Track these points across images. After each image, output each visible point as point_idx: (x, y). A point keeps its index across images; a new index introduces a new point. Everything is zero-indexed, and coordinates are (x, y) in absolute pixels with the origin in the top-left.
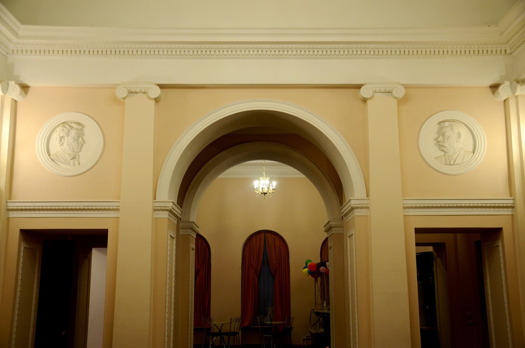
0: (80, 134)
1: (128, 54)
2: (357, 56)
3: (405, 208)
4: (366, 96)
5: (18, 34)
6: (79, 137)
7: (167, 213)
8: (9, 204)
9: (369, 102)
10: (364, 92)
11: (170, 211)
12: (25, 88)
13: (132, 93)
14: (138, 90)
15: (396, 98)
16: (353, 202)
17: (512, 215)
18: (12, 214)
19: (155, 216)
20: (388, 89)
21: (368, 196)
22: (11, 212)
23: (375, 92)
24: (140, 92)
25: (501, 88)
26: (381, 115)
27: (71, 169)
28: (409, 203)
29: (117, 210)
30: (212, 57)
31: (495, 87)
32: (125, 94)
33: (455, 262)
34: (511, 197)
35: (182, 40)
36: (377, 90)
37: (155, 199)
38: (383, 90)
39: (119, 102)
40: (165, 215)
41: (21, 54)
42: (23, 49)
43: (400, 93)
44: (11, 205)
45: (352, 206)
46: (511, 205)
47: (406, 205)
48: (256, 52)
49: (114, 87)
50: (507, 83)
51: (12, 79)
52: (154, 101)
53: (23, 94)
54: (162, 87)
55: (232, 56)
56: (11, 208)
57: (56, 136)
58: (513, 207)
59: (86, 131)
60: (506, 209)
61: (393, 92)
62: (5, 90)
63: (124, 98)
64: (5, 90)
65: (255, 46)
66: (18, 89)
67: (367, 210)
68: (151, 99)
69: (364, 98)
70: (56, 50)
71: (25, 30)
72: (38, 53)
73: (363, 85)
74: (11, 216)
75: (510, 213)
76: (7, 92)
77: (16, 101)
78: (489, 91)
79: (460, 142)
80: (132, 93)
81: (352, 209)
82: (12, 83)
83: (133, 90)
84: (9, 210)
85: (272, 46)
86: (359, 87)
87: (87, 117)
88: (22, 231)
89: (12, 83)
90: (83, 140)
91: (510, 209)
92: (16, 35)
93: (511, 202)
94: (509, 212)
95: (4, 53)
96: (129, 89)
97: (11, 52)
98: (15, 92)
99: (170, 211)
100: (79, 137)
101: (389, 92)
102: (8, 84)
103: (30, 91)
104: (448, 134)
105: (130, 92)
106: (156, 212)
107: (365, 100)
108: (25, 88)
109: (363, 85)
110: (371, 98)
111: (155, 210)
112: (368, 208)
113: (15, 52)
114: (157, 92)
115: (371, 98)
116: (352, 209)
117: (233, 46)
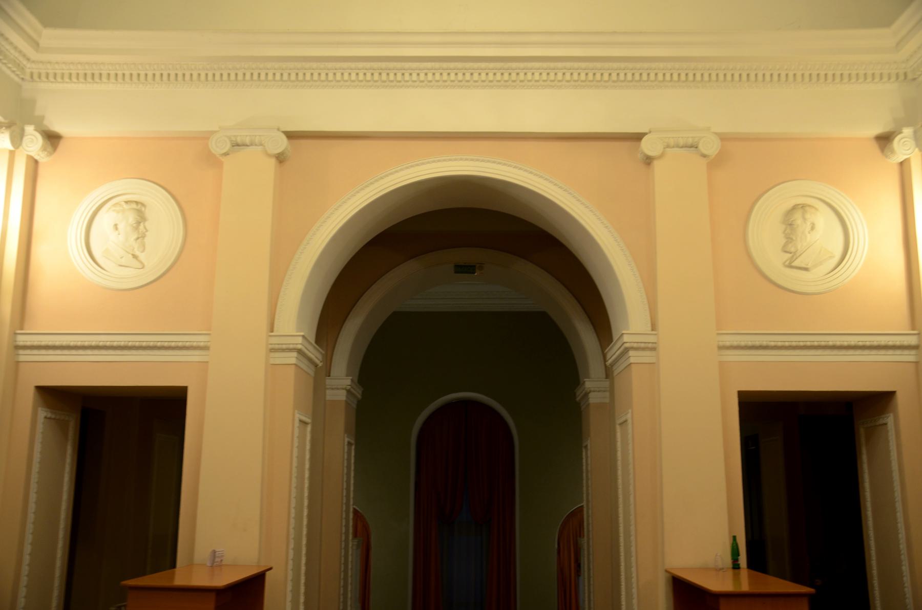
0: (141, 218)
1: (222, 80)
2: (549, 83)
3: (721, 348)
4: (650, 153)
5: (38, 44)
6: (139, 223)
7: (295, 354)
9: (656, 163)
10: (648, 146)
11: (300, 352)
12: (52, 139)
13: (238, 145)
14: (247, 141)
15: (704, 156)
16: (626, 338)
17: (917, 363)
18: (25, 356)
19: (272, 361)
20: (690, 141)
21: (654, 327)
22: (21, 352)
23: (668, 146)
24: (251, 145)
25: (896, 141)
26: (676, 188)
27: (130, 277)
28: (729, 340)
29: (206, 348)
30: (467, 84)
31: (884, 140)
32: (227, 147)
33: (804, 447)
34: (913, 329)
35: (276, 54)
36: (672, 142)
37: (272, 331)
38: (681, 142)
39: (213, 161)
40: (292, 358)
41: (67, 80)
42: (50, 71)
43: (711, 147)
44: (22, 340)
45: (627, 345)
47: (721, 344)
48: (453, 77)
49: (205, 137)
50: (907, 131)
51: (30, 123)
52: (273, 161)
53: (50, 149)
54: (291, 136)
55: (403, 83)
56: (21, 343)
57: (105, 220)
59: (148, 213)
60: (906, 352)
61: (701, 147)
62: (17, 139)
63: (226, 154)
64: (17, 139)
65: (376, 65)
66: (39, 140)
67: (653, 353)
68: (269, 155)
70: (104, 73)
71: (50, 36)
72: (89, 79)
73: (644, 134)
74: (22, 358)
75: (912, 358)
76: (20, 144)
77: (36, 162)
78: (874, 147)
79: (821, 234)
80: (238, 145)
81: (627, 350)
82: (30, 129)
83: (239, 140)
84: (18, 347)
85: (437, 65)
86: (637, 137)
87: (160, 189)
89: (30, 129)
90: (145, 228)
91: (913, 352)
92: (36, 45)
95: (16, 79)
96: (234, 139)
97: (28, 77)
98: (34, 143)
99: (300, 352)
100: (139, 223)
101: (691, 147)
102: (23, 130)
103: (62, 145)
104: (799, 221)
105: (236, 145)
106: (272, 355)
107: (648, 161)
108: (52, 139)
109: (644, 134)
110: (661, 156)
111: (273, 350)
112: (654, 349)
113: (36, 77)
114: (282, 144)
115: (661, 156)
116: (627, 350)
117: (459, 65)
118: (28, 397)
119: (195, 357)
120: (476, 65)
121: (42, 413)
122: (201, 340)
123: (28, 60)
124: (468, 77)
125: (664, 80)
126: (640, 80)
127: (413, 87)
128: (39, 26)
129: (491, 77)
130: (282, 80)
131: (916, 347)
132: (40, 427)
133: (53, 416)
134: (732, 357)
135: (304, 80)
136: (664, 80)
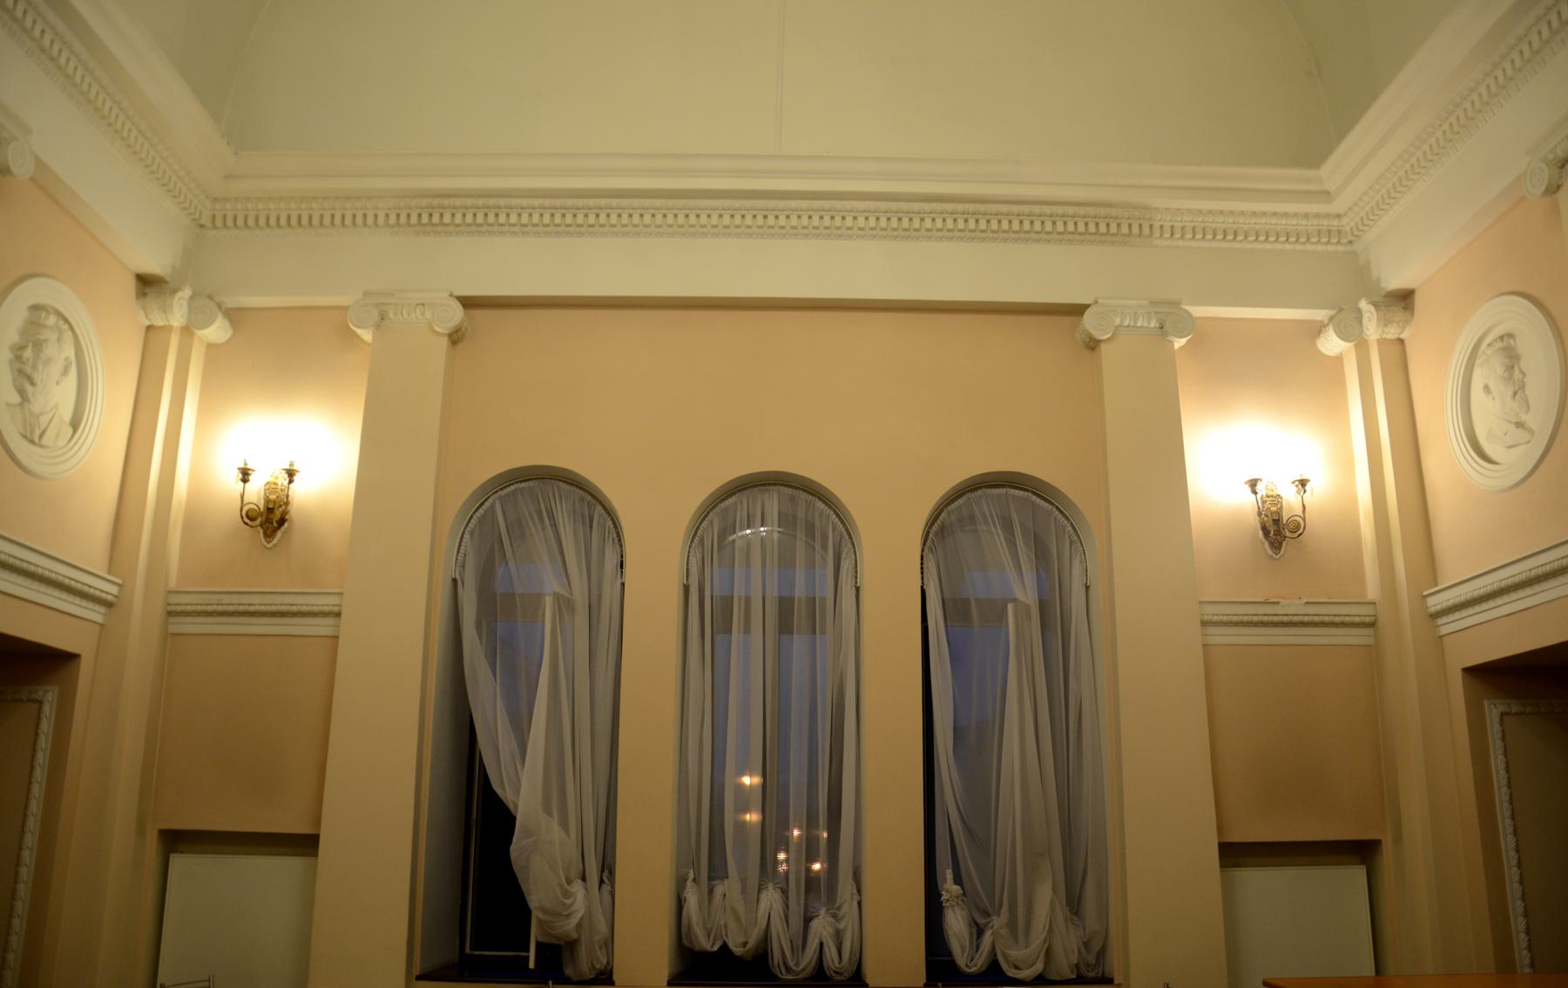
2: (1055, 236)
8: (1431, 601)
9: (1103, 347)
10: (1089, 321)
17: (102, 625)
18: (1447, 626)
22: (1440, 621)
44: (1436, 603)
46: (110, 598)
48: (827, 221)
54: (468, 303)
55: (619, 229)
58: (1372, 625)
69: (1091, 338)
73: (1087, 306)
74: (1444, 630)
75: (99, 618)
86: (1078, 310)
88: (1469, 671)
91: (103, 610)
92: (1326, 196)
93: (114, 590)
94: (95, 614)
102: (1359, 311)
103: (1419, 300)
106: (171, 620)
107: (1093, 345)
109: (1087, 306)
114: (457, 313)
118: (1457, 682)
119: (322, 627)
120: (648, 202)
121: (1493, 710)
122: (327, 603)
123: (1339, 216)
124: (614, 219)
125: (1130, 234)
126: (1108, 233)
127: (479, 233)
128: (1308, 173)
129: (816, 221)
130: (420, 223)
131: (108, 605)
132: (1493, 730)
133: (1515, 709)
134: (1219, 637)
135: (441, 223)
136: (398, 224)
